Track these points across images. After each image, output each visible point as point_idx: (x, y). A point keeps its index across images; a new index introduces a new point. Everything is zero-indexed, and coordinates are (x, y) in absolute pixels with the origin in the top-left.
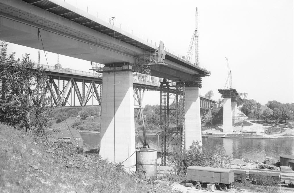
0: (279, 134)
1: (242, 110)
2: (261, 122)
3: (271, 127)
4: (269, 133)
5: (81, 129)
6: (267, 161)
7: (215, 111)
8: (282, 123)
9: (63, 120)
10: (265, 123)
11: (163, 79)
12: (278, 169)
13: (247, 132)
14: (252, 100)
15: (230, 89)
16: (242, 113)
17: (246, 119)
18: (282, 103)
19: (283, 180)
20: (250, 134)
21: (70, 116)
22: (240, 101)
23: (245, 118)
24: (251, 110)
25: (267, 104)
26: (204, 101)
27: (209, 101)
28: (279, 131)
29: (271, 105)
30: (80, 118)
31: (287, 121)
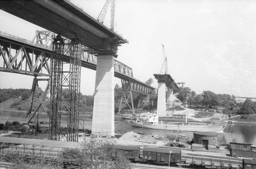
0: (208, 118)
1: (178, 97)
2: (193, 107)
3: (201, 112)
4: (199, 117)
5: (19, 109)
6: (180, 139)
7: (153, 97)
8: (211, 108)
9: (4, 101)
10: (196, 108)
11: (56, 35)
12: (189, 147)
13: (178, 115)
14: (188, 87)
15: (165, 74)
16: (178, 99)
17: (181, 104)
18: (215, 93)
19: (185, 159)
20: (180, 117)
21: (11, 96)
22: (177, 88)
23: (180, 104)
24: (186, 97)
25: (202, 94)
26: (138, 86)
27: (147, 87)
28: (208, 115)
29: (206, 94)
30: (21, 99)
31: (216, 106)
